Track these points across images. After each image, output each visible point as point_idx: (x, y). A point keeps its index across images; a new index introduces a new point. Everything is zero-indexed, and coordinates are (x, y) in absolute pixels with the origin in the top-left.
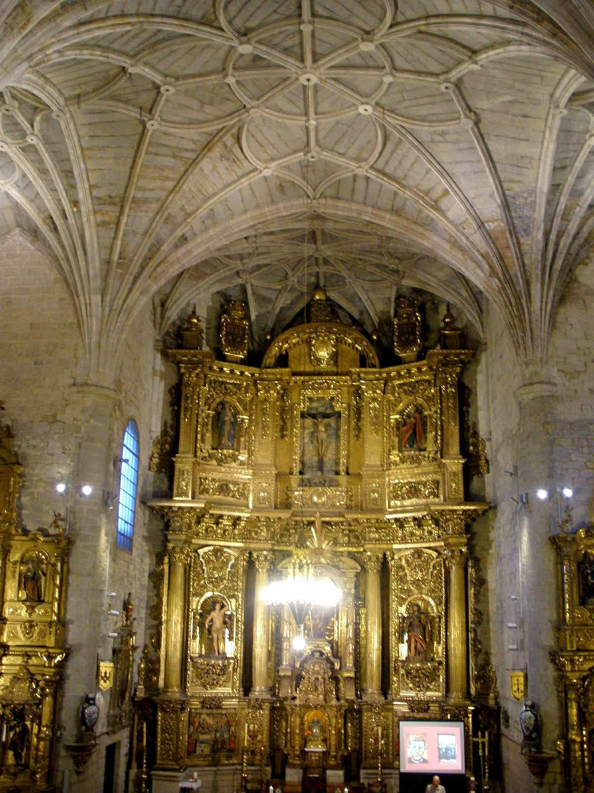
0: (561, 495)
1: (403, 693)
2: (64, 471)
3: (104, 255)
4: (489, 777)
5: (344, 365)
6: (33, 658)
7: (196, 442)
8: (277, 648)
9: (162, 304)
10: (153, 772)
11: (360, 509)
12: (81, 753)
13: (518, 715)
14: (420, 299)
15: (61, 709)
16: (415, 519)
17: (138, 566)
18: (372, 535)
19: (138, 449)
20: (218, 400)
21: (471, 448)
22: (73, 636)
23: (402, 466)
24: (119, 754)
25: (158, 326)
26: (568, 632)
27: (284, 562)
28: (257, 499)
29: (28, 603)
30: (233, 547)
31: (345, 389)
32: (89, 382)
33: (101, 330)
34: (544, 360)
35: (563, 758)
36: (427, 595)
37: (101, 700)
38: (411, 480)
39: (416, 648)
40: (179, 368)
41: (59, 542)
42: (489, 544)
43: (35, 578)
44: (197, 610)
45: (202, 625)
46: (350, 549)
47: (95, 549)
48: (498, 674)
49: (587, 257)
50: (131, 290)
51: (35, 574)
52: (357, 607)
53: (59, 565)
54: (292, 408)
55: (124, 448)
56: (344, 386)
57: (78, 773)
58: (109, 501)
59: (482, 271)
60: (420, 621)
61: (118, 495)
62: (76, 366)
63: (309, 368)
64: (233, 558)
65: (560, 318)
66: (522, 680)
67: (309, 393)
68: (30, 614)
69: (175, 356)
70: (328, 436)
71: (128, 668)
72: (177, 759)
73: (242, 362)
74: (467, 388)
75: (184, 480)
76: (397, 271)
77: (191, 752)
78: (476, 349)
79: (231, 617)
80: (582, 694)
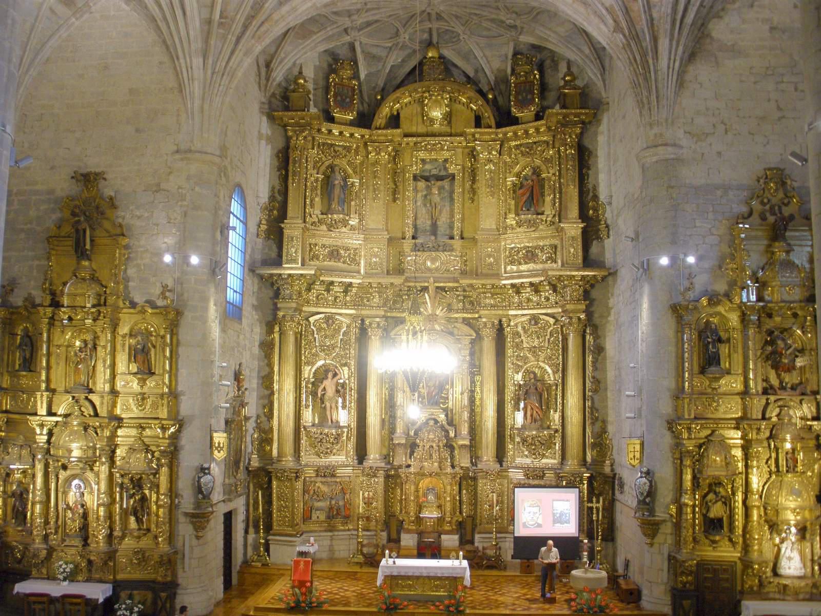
0: (684, 261)
1: (519, 460)
2: (170, 241)
3: (205, 14)
4: (602, 540)
5: (458, 127)
6: (147, 430)
7: (305, 208)
8: (391, 416)
9: (267, 64)
10: (270, 537)
11: (477, 275)
12: (199, 519)
13: (633, 482)
14: (538, 57)
15: (177, 478)
16: (531, 284)
17: (248, 335)
18: (487, 301)
19: (246, 216)
20: (327, 164)
21: (591, 212)
22: (185, 408)
23: (518, 230)
24: (236, 520)
25: (263, 89)
26: (686, 401)
27: (397, 328)
28: (369, 264)
29: (139, 376)
30: (345, 314)
31: (460, 150)
32: (193, 148)
33: (204, 94)
34: (670, 121)
35: (674, 520)
36: (544, 362)
37: (216, 470)
38: (527, 244)
39: (532, 416)
40: (286, 131)
41: (167, 313)
42: (608, 310)
43: (145, 351)
44: (309, 378)
45: (314, 394)
46: (465, 315)
47: (204, 320)
48: (615, 442)
49: (723, 9)
50: (232, 53)
51: (144, 347)
52: (472, 375)
53: (168, 336)
54: (404, 171)
55: (231, 215)
56: (458, 147)
57: (198, 538)
58: (217, 270)
59: (605, 24)
60: (536, 389)
61: (226, 264)
62: (179, 132)
63: (421, 129)
64: (345, 325)
65: (688, 77)
66: (638, 447)
67: (422, 155)
68: (142, 387)
69: (282, 119)
70: (442, 199)
71: (241, 438)
72: (293, 525)
73: (352, 124)
74: (587, 149)
75: (293, 247)
76: (515, 27)
77: (307, 518)
78: (598, 110)
79: (343, 385)
80: (697, 461)
